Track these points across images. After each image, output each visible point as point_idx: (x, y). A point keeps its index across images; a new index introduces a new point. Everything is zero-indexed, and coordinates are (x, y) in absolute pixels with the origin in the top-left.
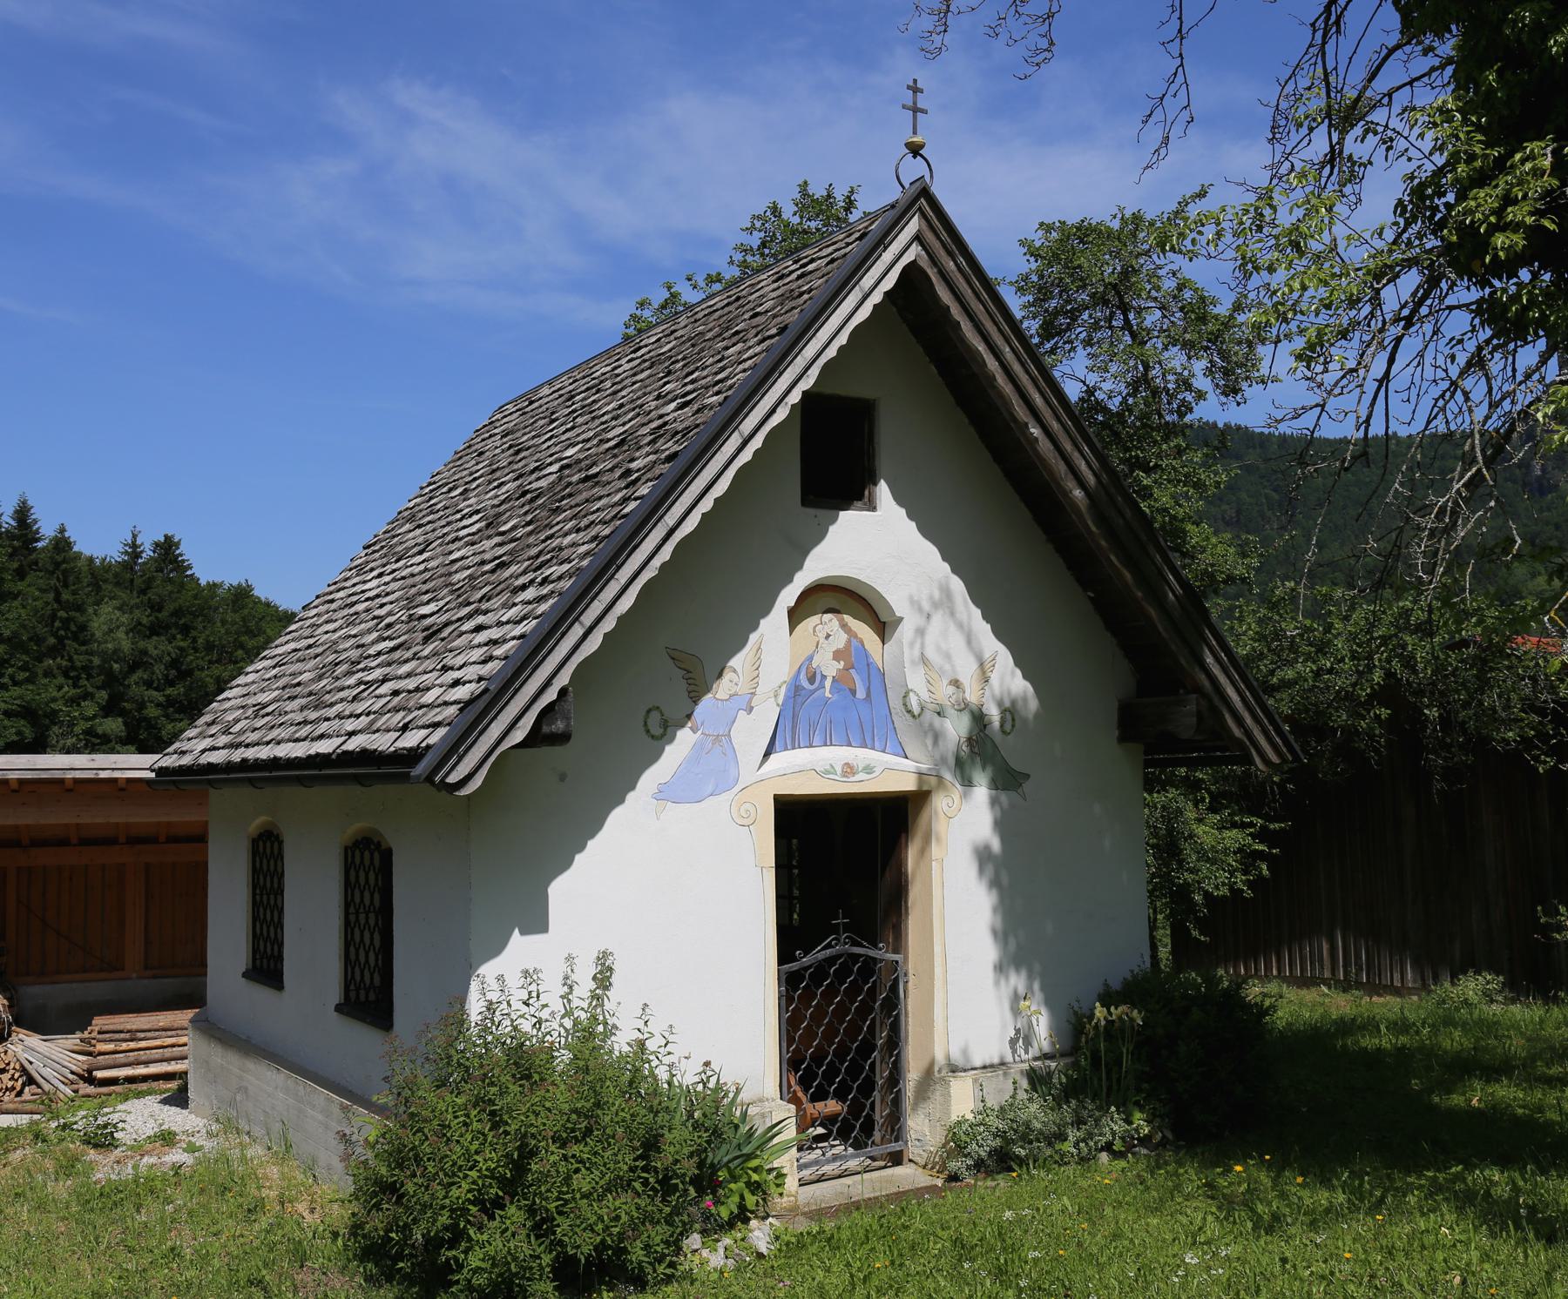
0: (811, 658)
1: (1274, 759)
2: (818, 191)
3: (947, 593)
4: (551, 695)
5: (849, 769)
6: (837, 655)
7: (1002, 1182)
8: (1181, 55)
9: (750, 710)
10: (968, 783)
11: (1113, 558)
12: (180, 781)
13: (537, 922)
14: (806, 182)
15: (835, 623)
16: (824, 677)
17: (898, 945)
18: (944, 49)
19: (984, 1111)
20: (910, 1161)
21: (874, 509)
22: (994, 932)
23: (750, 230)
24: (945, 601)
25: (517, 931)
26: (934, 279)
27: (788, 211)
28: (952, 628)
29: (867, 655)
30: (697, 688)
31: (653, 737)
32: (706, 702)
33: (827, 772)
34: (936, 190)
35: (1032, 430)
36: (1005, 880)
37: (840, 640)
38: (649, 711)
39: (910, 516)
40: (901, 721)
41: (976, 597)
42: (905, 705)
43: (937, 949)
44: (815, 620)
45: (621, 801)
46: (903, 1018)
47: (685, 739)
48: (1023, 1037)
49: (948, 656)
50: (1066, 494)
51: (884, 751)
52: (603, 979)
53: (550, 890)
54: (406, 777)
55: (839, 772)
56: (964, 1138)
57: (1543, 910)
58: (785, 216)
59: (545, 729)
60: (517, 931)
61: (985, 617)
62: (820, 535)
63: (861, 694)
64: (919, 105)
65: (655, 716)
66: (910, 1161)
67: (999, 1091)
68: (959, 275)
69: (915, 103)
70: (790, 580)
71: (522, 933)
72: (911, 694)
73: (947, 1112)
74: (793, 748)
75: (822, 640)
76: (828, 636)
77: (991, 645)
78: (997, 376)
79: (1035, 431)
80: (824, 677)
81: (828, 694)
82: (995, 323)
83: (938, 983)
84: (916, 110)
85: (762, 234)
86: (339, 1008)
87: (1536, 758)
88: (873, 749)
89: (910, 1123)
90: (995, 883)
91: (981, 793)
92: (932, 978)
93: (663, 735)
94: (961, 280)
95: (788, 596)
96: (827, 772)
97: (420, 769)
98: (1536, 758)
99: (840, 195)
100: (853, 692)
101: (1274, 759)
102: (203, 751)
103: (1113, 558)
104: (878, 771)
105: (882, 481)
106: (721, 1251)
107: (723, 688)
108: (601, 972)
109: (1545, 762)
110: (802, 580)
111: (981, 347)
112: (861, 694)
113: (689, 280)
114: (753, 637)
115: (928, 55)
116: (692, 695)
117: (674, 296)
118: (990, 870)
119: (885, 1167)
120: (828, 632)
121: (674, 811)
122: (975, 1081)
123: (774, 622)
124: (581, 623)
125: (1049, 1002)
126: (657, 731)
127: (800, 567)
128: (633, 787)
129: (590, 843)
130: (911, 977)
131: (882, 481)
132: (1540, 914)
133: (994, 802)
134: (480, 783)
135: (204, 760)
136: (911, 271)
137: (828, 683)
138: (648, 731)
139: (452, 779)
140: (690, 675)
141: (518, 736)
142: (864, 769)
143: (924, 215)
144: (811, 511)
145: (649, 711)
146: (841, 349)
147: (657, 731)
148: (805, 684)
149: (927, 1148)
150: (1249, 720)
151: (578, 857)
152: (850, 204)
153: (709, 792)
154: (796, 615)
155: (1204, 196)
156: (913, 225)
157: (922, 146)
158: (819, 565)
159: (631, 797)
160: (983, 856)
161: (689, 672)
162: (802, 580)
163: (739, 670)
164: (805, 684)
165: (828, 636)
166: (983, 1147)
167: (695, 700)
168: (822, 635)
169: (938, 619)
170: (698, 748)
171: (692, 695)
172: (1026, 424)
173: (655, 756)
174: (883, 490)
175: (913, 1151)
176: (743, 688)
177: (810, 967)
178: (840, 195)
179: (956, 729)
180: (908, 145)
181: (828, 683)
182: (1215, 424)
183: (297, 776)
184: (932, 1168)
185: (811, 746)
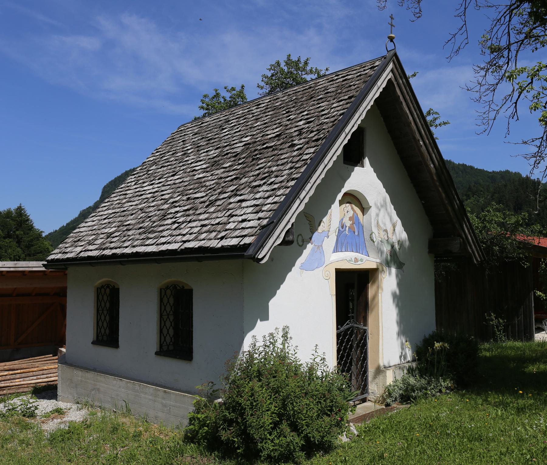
0: (342, 219)
1: (479, 259)
2: (294, 58)
4: (289, 226)
5: (356, 260)
6: (350, 219)
7: (404, 406)
8: (465, 21)
9: (328, 237)
11: (440, 189)
12: (66, 264)
13: (265, 317)
14: (290, 55)
15: (350, 207)
16: (346, 226)
17: (365, 323)
18: (386, 7)
19: (396, 381)
20: (369, 400)
21: (363, 167)
22: (397, 322)
23: (270, 70)
25: (259, 320)
26: (396, 85)
27: (283, 65)
29: (359, 219)
31: (299, 245)
32: (315, 234)
33: (350, 261)
34: (398, 54)
35: (421, 143)
36: (400, 304)
37: (351, 213)
38: (298, 236)
39: (375, 171)
40: (368, 243)
41: (393, 202)
42: (371, 238)
43: (380, 325)
45: (290, 270)
46: (368, 349)
47: (309, 246)
48: (403, 356)
49: (385, 225)
50: (427, 166)
51: (362, 254)
52: (285, 336)
53: (270, 304)
54: (242, 256)
55: (353, 261)
56: (391, 391)
57: (487, 315)
58: (281, 66)
59: (287, 239)
60: (259, 320)
61: (395, 209)
62: (348, 176)
63: (356, 233)
64: (393, 24)
65: (300, 237)
66: (369, 400)
67: (400, 375)
68: (402, 85)
69: (392, 22)
70: (340, 191)
71: (261, 321)
72: (373, 234)
73: (386, 383)
74: (337, 252)
75: (346, 213)
76: (348, 212)
77: (396, 218)
78: (412, 122)
79: (421, 143)
80: (346, 226)
81: (347, 233)
82: (412, 104)
83: (380, 337)
84: (392, 25)
85: (274, 71)
86: (157, 353)
87: (523, 263)
88: (359, 253)
89: (370, 387)
90: (397, 306)
91: (394, 270)
92: (378, 335)
93: (303, 245)
94: (403, 87)
95: (340, 197)
96: (350, 261)
97: (250, 252)
98: (523, 263)
99: (302, 60)
100: (354, 232)
101: (479, 259)
102: (81, 252)
103: (440, 189)
104: (364, 260)
105: (366, 157)
106: (345, 435)
107: (320, 229)
108: (284, 334)
109: (526, 264)
110: (344, 191)
111: (408, 112)
112: (356, 233)
113: (225, 88)
114: (329, 211)
115: (380, 9)
116: (311, 230)
117: (217, 94)
118: (396, 300)
119: (360, 403)
120: (349, 209)
121: (306, 273)
122: (393, 371)
123: (335, 206)
124: (299, 199)
125: (411, 344)
126: (301, 243)
128: (294, 266)
129: (282, 286)
130: (370, 335)
131: (366, 157)
132: (486, 316)
133: (397, 276)
134: (267, 259)
135: (82, 255)
136: (390, 81)
137: (347, 229)
138: (298, 243)
139: (260, 257)
140: (310, 223)
141: (279, 241)
142: (361, 260)
143: (394, 63)
144: (346, 166)
145: (298, 236)
146: (372, 106)
147: (301, 243)
149: (376, 395)
150: (473, 247)
151: (278, 291)
152: (306, 63)
153: (316, 267)
154: (341, 203)
155: (415, 76)
156: (391, 66)
157: (394, 38)
158: (348, 186)
159: (293, 269)
160: (394, 295)
161: (310, 222)
162: (344, 191)
163: (325, 222)
165: (348, 212)
166: (397, 393)
167: (313, 233)
168: (346, 211)
169: (382, 211)
170: (313, 250)
171: (311, 230)
172: (419, 140)
173: (300, 254)
174: (367, 161)
175: (371, 397)
176: (326, 229)
177: (342, 332)
178: (302, 60)
179: (386, 249)
180: (389, 37)
181: (347, 229)
183: (155, 259)
184: (378, 402)
185: (342, 251)
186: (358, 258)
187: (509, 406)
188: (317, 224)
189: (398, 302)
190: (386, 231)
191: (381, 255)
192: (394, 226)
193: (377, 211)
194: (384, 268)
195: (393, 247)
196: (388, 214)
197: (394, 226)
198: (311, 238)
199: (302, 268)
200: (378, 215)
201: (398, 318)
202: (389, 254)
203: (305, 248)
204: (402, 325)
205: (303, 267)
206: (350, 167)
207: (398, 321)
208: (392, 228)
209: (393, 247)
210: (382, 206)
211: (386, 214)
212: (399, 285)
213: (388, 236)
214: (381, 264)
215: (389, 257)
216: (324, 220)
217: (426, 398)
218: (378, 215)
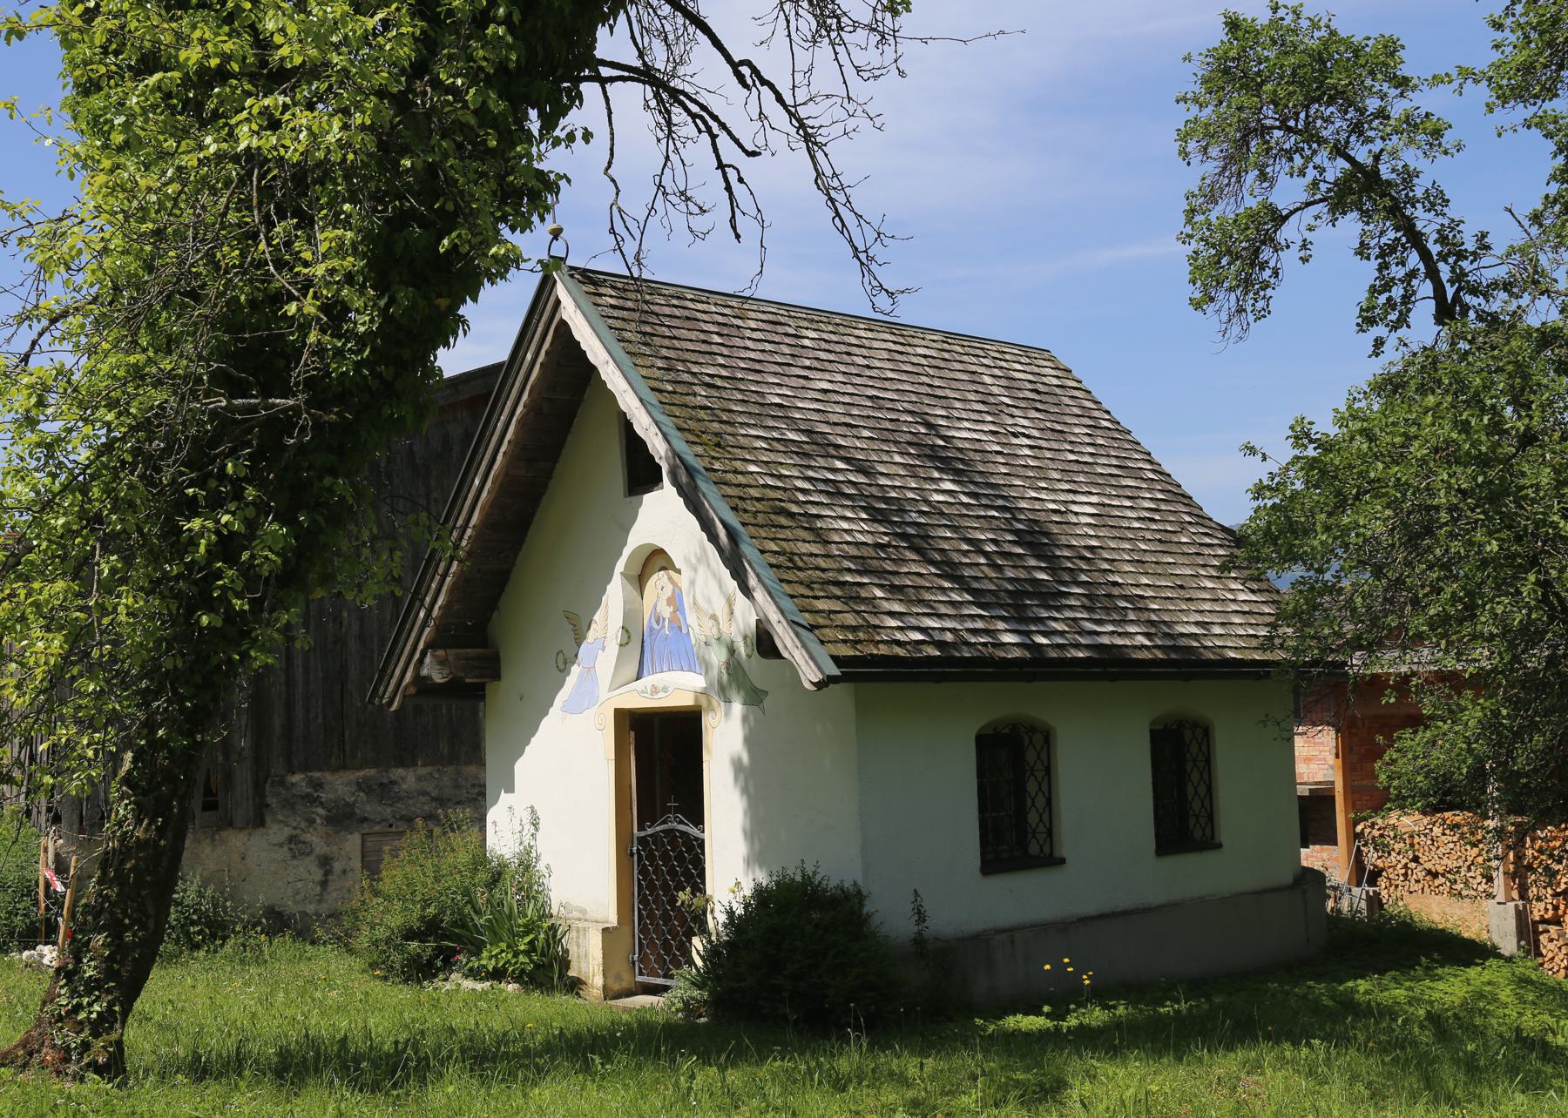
3: (704, 550)
10: (728, 701)
22: (745, 833)
24: (703, 558)
28: (710, 577)
30: (579, 639)
33: (643, 692)
36: (752, 790)
44: (655, 577)
47: (575, 669)
49: (709, 601)
90: (745, 791)
91: (737, 708)
104: (670, 690)
107: (591, 635)
118: (741, 778)
126: (562, 667)
127: (625, 544)
133: (745, 719)
147: (562, 667)
148: (655, 626)
160: (737, 766)
164: (655, 626)
167: (579, 646)
169: (702, 569)
170: (581, 676)
179: (718, 657)
182: (447, 344)
186: (657, 684)
187: (344, 259)
188: (585, 628)
189: (746, 782)
190: (714, 617)
191: (707, 672)
192: (730, 603)
193: (692, 574)
194: (715, 703)
195: (732, 651)
196: (714, 575)
197: (730, 603)
198: (576, 656)
199: (565, 709)
200: (692, 583)
201: (748, 821)
202: (724, 671)
203: (569, 673)
204: (756, 840)
205: (568, 709)
206: (634, 499)
207: (748, 826)
208: (726, 610)
209: (732, 651)
210: (699, 560)
211: (710, 577)
212: (750, 741)
213: (719, 630)
214: (704, 693)
215: (725, 677)
216: (596, 617)
217: (1425, 348)
218: (692, 583)
